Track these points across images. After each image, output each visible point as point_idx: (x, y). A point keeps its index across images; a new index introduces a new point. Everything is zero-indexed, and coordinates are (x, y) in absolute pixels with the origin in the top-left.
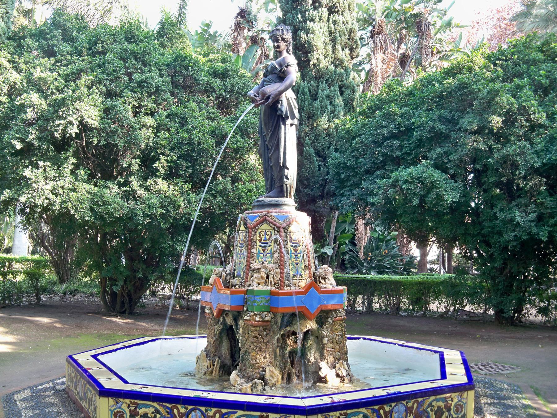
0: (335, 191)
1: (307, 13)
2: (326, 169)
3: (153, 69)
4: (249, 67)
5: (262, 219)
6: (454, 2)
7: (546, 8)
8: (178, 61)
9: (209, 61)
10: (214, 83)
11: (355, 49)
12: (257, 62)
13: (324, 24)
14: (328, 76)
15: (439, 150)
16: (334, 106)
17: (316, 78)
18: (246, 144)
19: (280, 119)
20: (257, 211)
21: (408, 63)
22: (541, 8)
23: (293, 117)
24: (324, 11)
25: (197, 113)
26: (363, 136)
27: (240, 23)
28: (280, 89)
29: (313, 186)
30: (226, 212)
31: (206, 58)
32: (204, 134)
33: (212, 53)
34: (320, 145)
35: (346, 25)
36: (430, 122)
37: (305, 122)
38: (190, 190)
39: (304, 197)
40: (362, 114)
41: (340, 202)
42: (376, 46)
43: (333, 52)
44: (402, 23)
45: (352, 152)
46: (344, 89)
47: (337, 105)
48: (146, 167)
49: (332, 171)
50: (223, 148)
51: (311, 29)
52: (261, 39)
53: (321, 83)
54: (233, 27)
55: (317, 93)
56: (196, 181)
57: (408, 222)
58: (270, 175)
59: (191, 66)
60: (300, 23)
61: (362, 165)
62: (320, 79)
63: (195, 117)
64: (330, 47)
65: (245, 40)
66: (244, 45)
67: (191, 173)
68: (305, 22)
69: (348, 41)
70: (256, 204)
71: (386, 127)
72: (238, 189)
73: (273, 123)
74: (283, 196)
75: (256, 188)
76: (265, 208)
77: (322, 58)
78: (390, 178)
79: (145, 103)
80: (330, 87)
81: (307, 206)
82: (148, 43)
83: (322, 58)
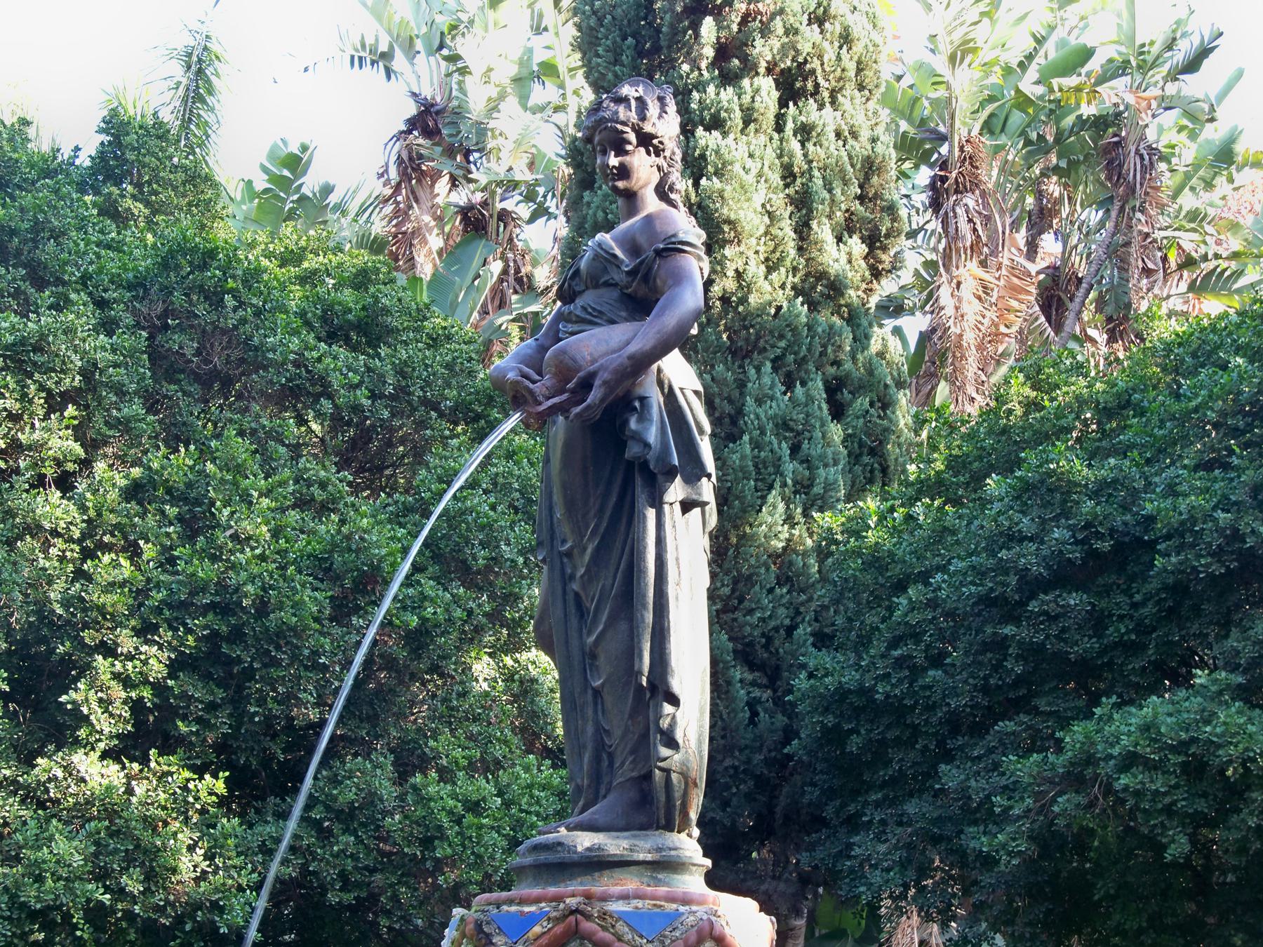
1: (695, 95)
2: (781, 719)
3: (73, 296)
5: (559, 929)
6: (1239, 75)
8: (178, 267)
11: (887, 236)
12: (484, 305)
14: (783, 344)
16: (806, 461)
18: (458, 613)
19: (639, 481)
20: (536, 891)
21: (1073, 306)
23: (694, 471)
24: (766, 91)
25: (255, 483)
26: (939, 577)
27: (420, 157)
28: (633, 348)
29: (727, 787)
30: (373, 898)
32: (283, 568)
35: (851, 142)
36: (1221, 515)
38: (223, 802)
40: (925, 488)
41: (846, 852)
42: (957, 236)
43: (800, 249)
44: (1047, 152)
45: (895, 643)
48: (37, 708)
49: (809, 728)
51: (711, 157)
53: (753, 371)
54: (393, 174)
55: (740, 412)
57: (1141, 931)
58: (590, 729)
59: (233, 292)
61: (937, 697)
62: (748, 355)
64: (786, 230)
65: (439, 219)
66: (435, 242)
67: (226, 729)
69: (857, 206)
71: (1031, 539)
72: (423, 800)
73: (606, 496)
75: (500, 794)
76: (572, 877)
77: (756, 270)
78: (1059, 747)
79: (37, 435)
80: (789, 386)
82: (56, 192)
83: (756, 270)
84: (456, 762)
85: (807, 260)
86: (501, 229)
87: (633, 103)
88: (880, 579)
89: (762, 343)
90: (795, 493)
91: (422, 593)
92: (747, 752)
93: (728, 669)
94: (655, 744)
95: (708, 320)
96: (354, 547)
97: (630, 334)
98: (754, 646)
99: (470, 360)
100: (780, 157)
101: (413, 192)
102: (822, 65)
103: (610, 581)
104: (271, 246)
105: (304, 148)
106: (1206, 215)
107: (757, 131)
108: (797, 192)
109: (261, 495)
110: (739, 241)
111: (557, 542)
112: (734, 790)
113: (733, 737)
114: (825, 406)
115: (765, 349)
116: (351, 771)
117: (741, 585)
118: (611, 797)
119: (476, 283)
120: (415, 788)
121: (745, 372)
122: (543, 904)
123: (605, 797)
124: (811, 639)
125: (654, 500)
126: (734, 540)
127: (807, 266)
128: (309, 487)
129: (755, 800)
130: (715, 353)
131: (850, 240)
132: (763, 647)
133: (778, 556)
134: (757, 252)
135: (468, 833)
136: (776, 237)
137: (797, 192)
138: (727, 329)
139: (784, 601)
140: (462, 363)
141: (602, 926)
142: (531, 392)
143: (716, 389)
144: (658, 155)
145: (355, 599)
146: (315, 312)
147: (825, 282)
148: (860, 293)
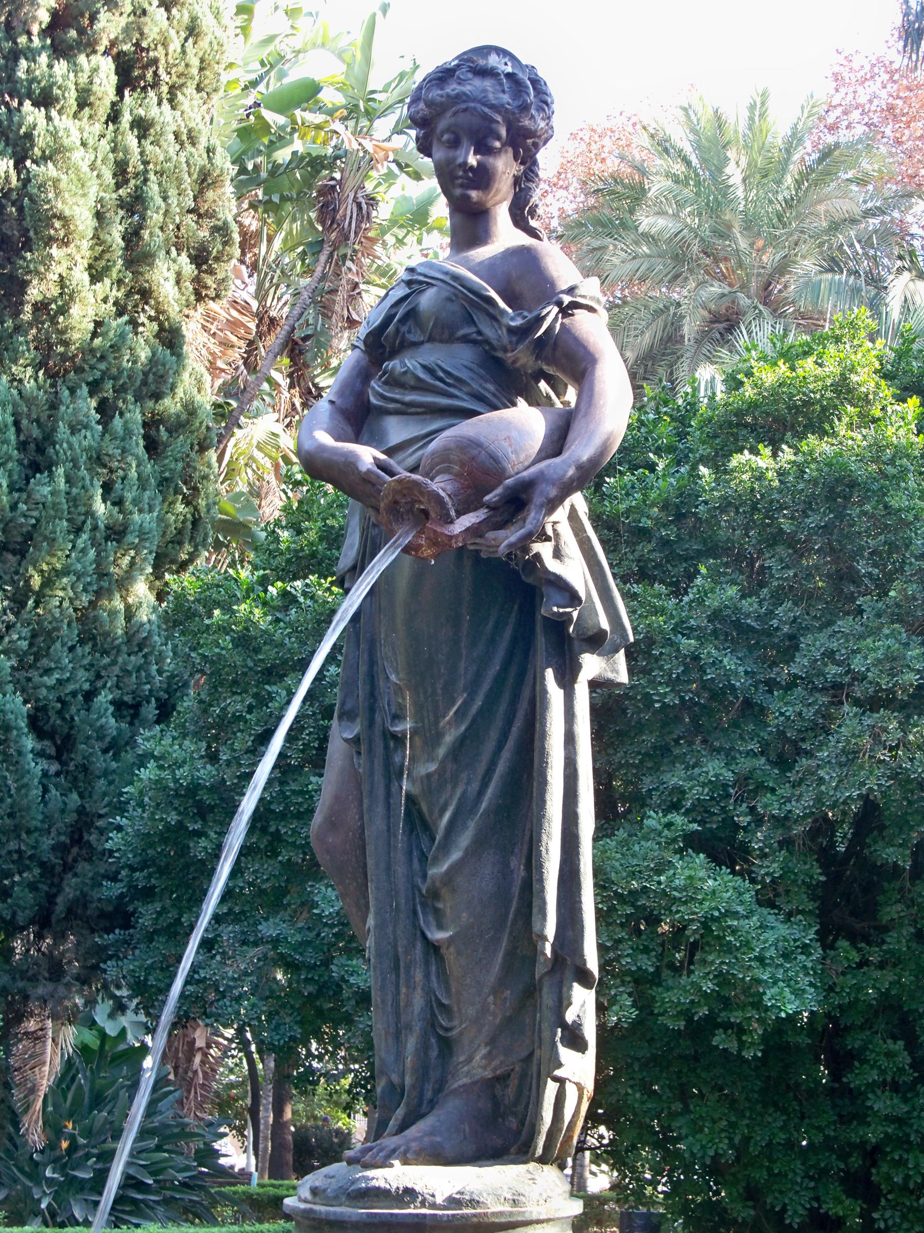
1: (23, 63)
7: (676, 216)
11: (217, 259)
13: (98, 128)
15: (714, 768)
22: (662, 213)
34: (50, 681)
55: (49, 437)
58: (418, 1001)
73: (484, 662)
77: (80, 276)
90: (107, 538)
92: (36, 834)
102: (167, 55)
103: (475, 786)
106: (395, 272)
107: (91, 117)
114: (142, 443)
143: (25, 409)
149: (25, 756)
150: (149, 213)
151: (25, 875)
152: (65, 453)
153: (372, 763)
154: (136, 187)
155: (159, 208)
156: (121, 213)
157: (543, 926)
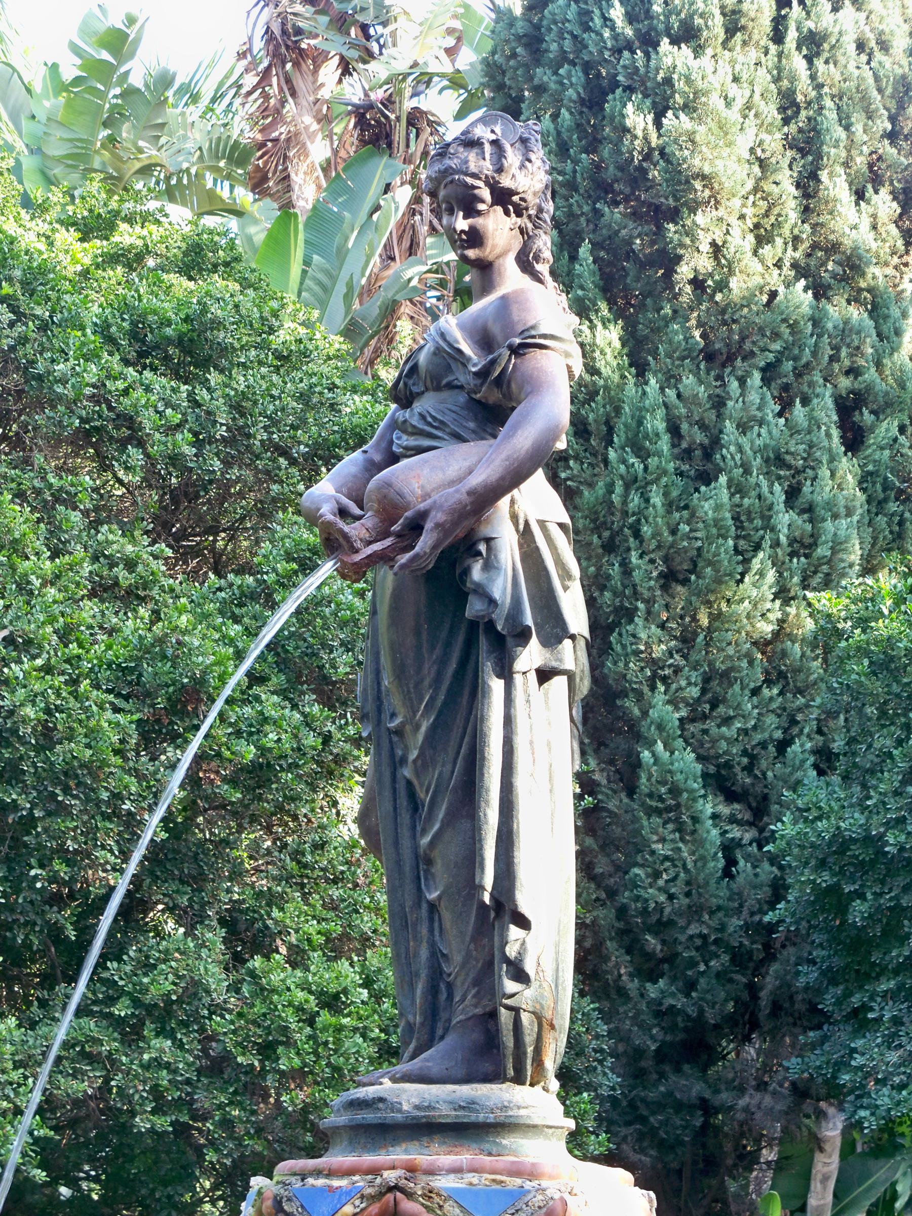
0: (819, 992)
2: (767, 870)
4: (344, 276)
9: (112, 259)
10: (138, 394)
12: (388, 247)
14: (777, 346)
16: (809, 510)
17: (710, 356)
18: (311, 740)
19: (483, 643)
27: (299, 31)
28: (477, 479)
29: (693, 964)
31: (97, 246)
32: (74, 682)
33: (130, 220)
35: (878, 56)
37: (649, 602)
39: (645, 1028)
43: (806, 211)
46: (867, 417)
47: (830, 505)
50: (187, 758)
51: (680, 85)
52: (415, 118)
53: (735, 384)
55: (716, 442)
56: (27, 944)
58: (424, 953)
60: (619, 51)
62: (730, 359)
63: (23, 587)
65: (325, 120)
68: (649, 42)
69: (888, 149)
70: (342, 1119)
72: (263, 992)
73: (443, 662)
74: (495, 1076)
76: (395, 1142)
80: (786, 406)
81: (662, 1075)
84: (309, 940)
85: (814, 226)
86: (412, 136)
87: (488, 148)
88: (895, 688)
89: (747, 346)
90: (792, 555)
91: (261, 713)
92: (720, 915)
93: (695, 800)
94: (500, 977)
95: (675, 312)
96: (170, 652)
97: (474, 459)
98: (732, 767)
99: (332, 387)
100: (777, 80)
101: (288, 81)
103: (449, 767)
104: (70, 208)
105: (131, 20)
107: (745, 43)
108: (800, 130)
109: (44, 585)
110: (717, 202)
111: (386, 716)
112: (702, 968)
113: (700, 894)
114: (835, 433)
115: (752, 354)
116: (167, 952)
117: (714, 683)
118: (449, 1039)
119: (375, 217)
120: (252, 973)
121: (724, 385)
122: (356, 1178)
123: (442, 1038)
124: (812, 759)
125: (502, 668)
126: (704, 621)
127: (813, 234)
128: (112, 566)
129: (731, 981)
130: (682, 359)
131: (875, 198)
132: (743, 769)
133: (767, 643)
134: (742, 217)
135: (322, 1037)
136: (769, 194)
137: (800, 130)
138: (700, 324)
139: (774, 705)
140: (321, 393)
141: (426, 1207)
142: (346, 536)
143: (683, 411)
144: (519, 214)
145: (172, 723)
146: (120, 327)
147: (837, 257)
148: (890, 271)
149: (703, 823)
150: (825, 148)
151: (712, 963)
152: (733, 458)
153: (380, 754)
154: (809, 119)
155: (837, 141)
156: (789, 154)
157: (482, 878)
